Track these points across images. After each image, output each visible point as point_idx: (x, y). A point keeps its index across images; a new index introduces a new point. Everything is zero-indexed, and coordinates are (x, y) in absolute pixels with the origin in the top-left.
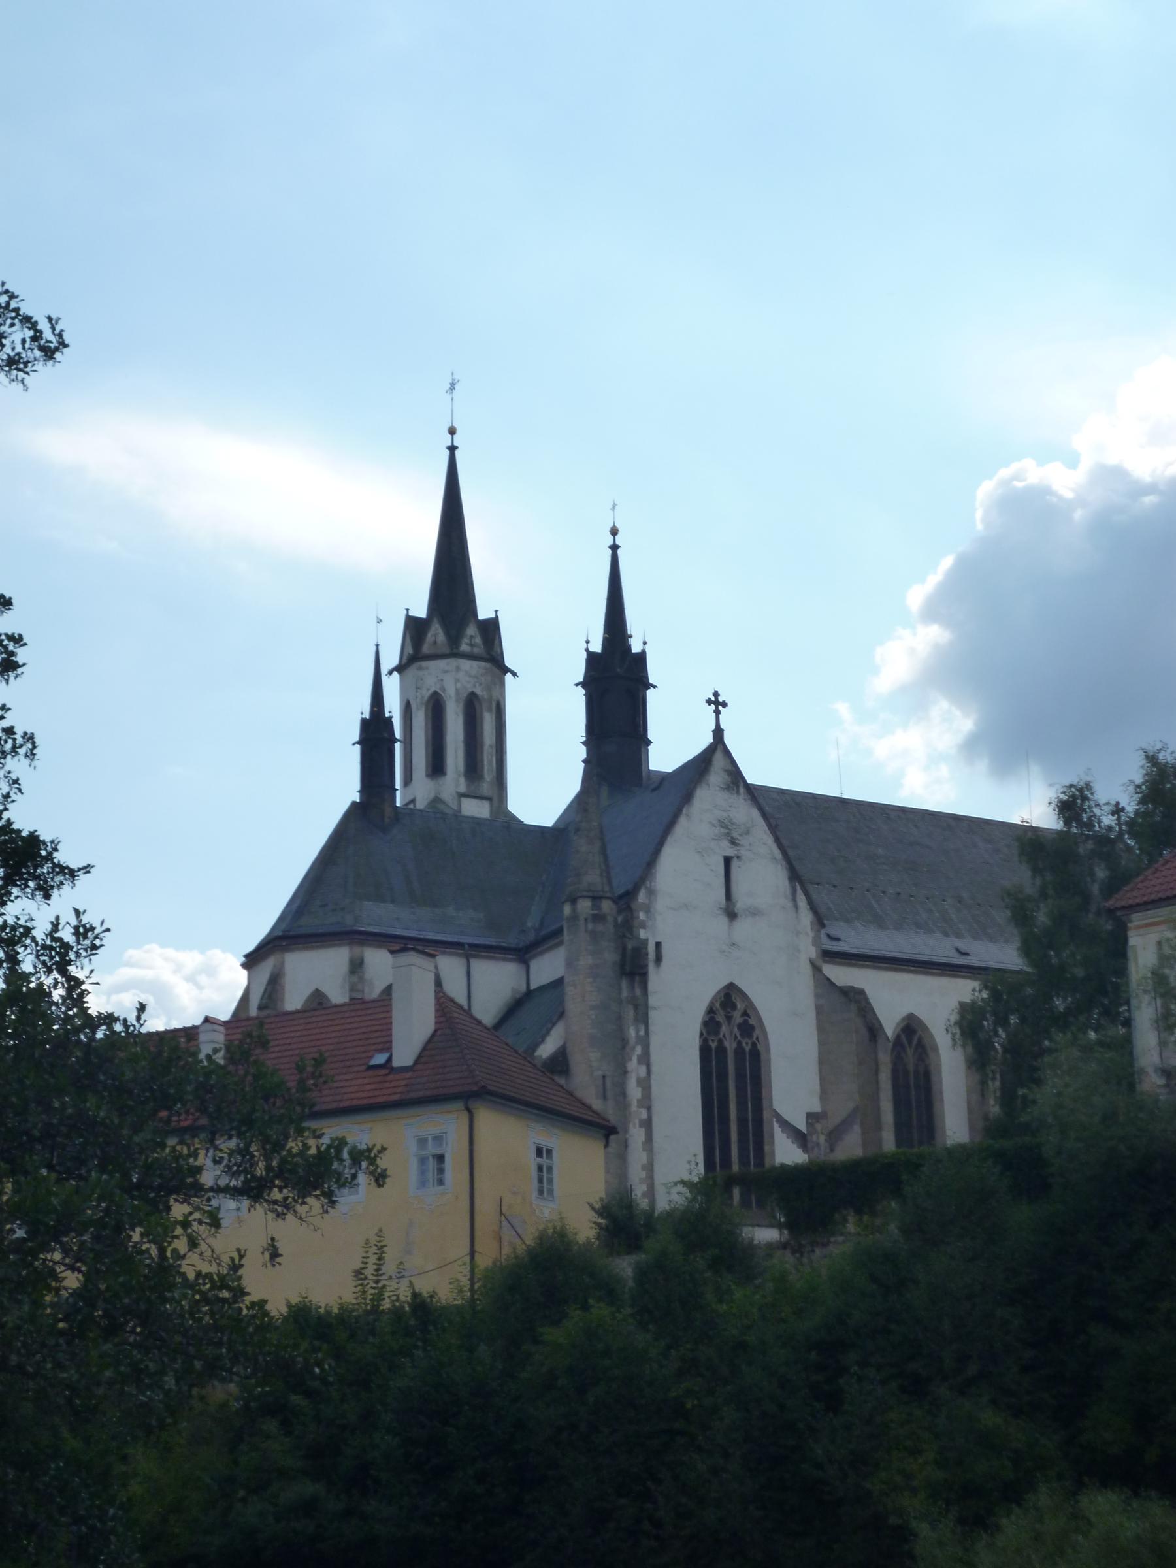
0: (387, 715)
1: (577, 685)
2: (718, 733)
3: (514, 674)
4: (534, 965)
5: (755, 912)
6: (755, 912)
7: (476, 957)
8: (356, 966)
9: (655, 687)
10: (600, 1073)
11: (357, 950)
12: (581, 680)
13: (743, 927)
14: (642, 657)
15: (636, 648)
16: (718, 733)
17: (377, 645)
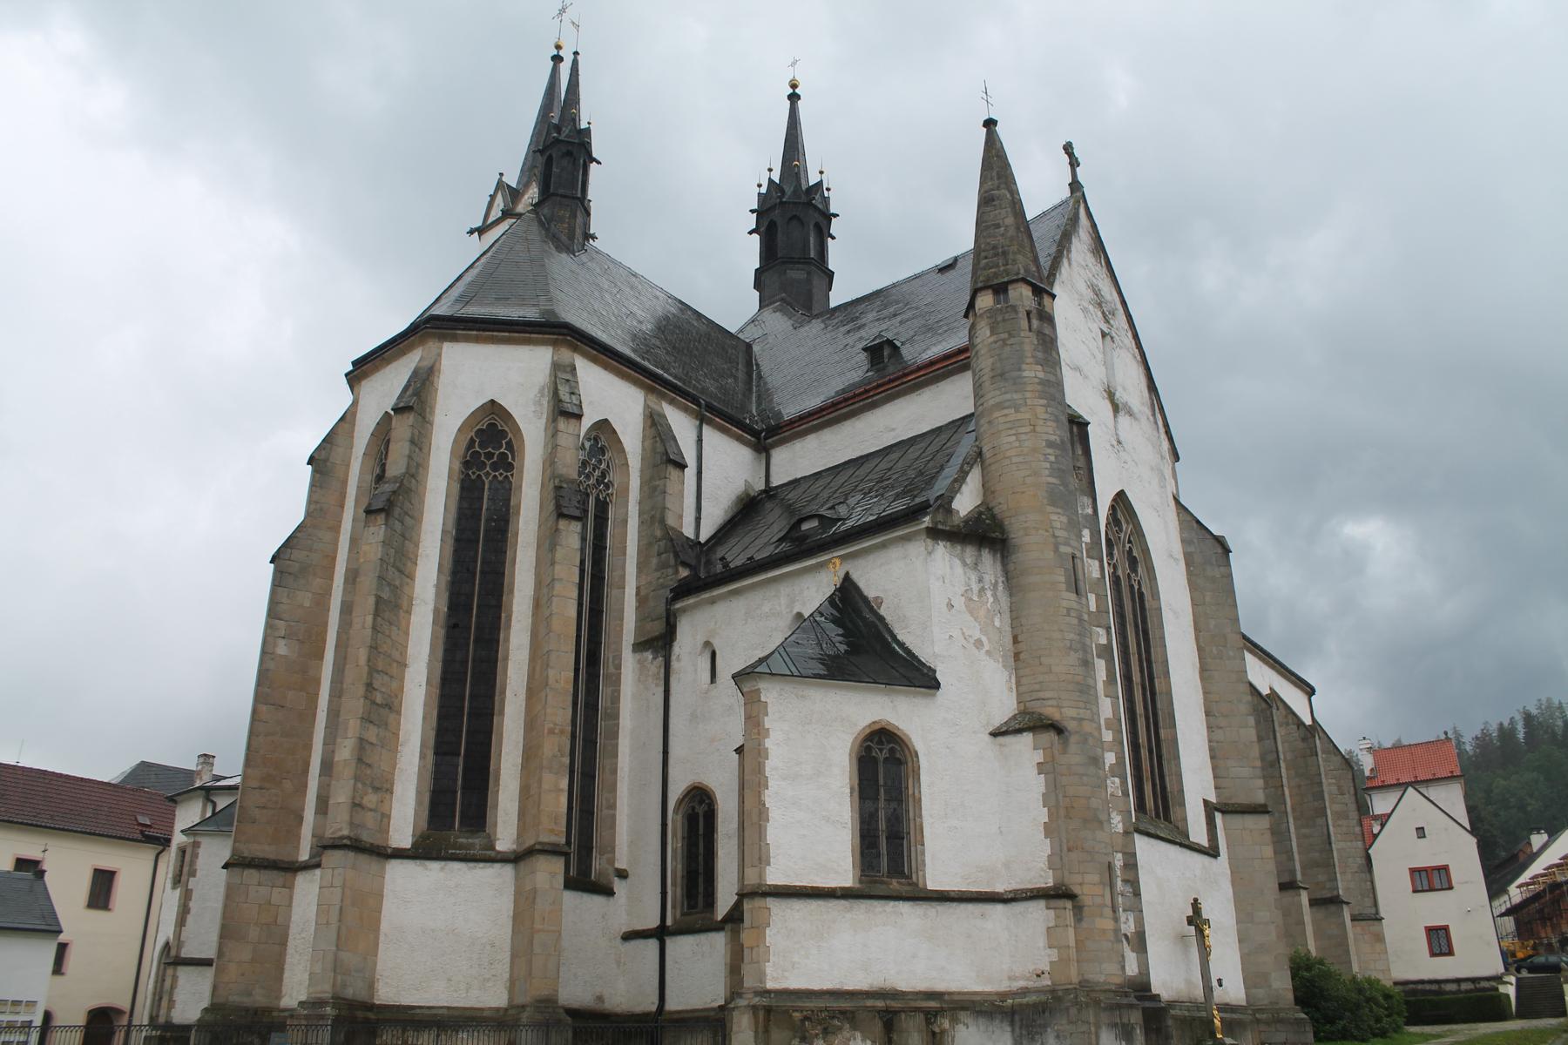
0: (584, 125)
1: (752, 211)
2: (1075, 186)
4: (780, 456)
5: (1130, 414)
6: (1130, 414)
7: (710, 423)
8: (563, 375)
10: (1068, 550)
11: (566, 355)
13: (1124, 420)
14: (588, 130)
16: (1075, 186)
17: (990, 124)
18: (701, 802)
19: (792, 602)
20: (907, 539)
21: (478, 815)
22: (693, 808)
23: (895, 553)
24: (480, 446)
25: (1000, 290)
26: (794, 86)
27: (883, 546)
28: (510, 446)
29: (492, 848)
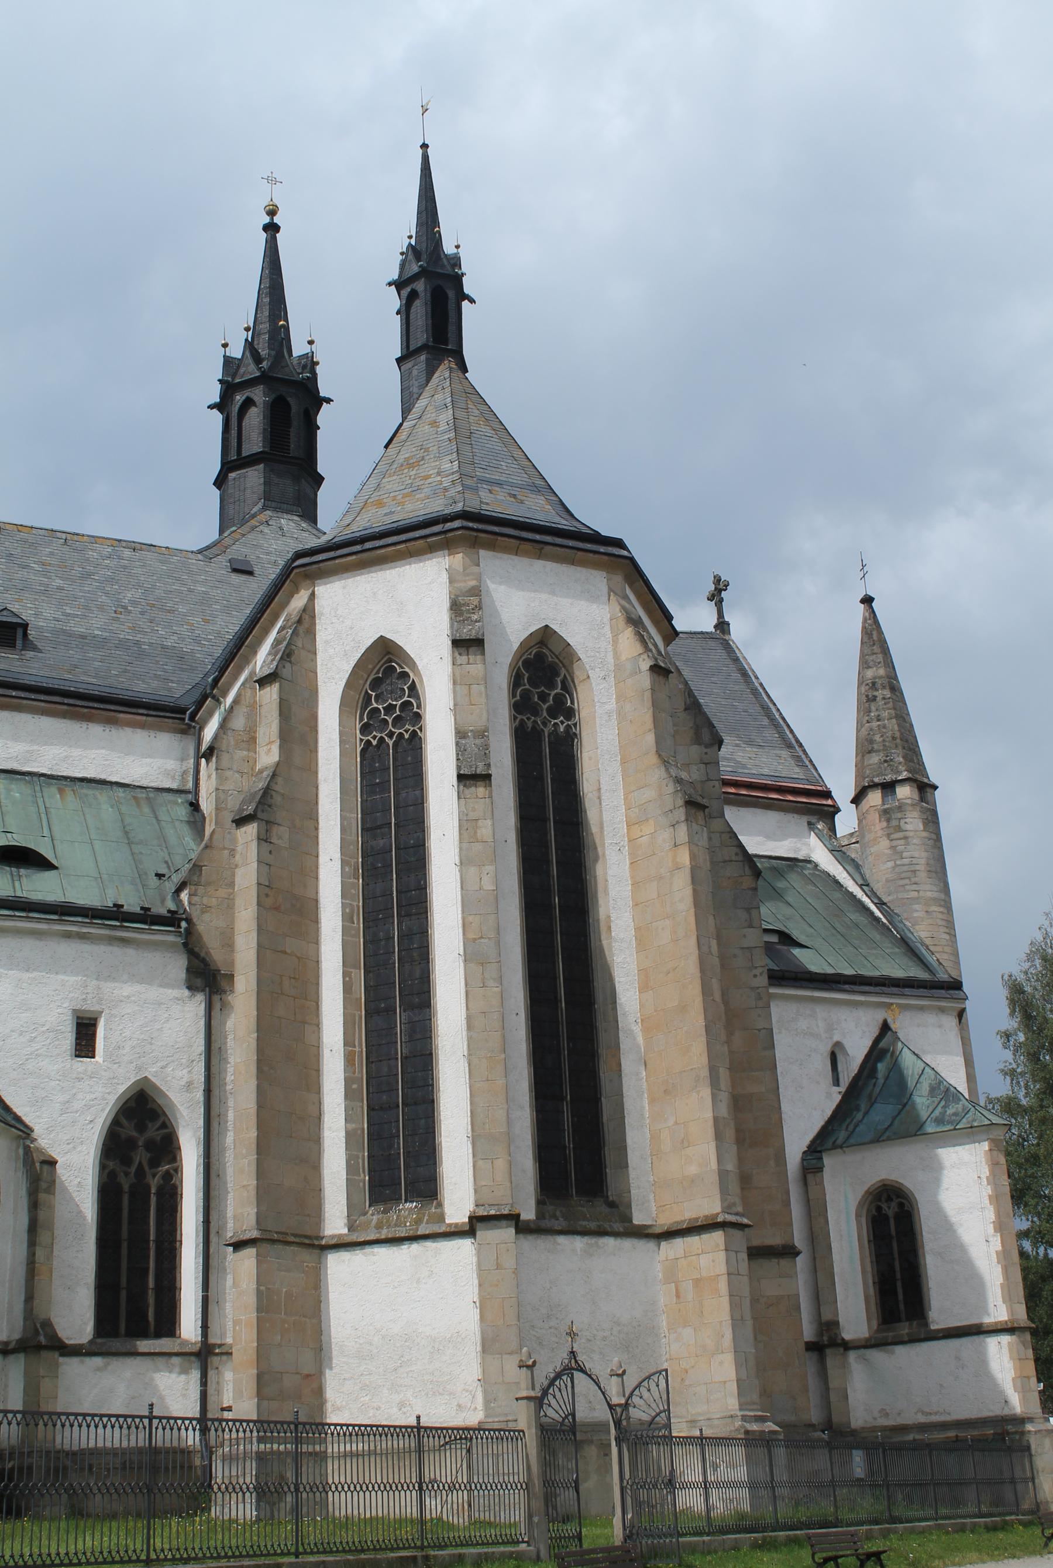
3: (472, 301)
9: (329, 401)
12: (217, 399)
15: (448, 248)
18: (889, 1199)
19: (830, 1029)
20: (942, 1010)
21: (426, 1187)
22: (879, 1209)
23: (930, 1018)
24: (532, 682)
25: (888, 787)
26: (272, 212)
27: (921, 1008)
28: (565, 687)
29: (627, 1218)
